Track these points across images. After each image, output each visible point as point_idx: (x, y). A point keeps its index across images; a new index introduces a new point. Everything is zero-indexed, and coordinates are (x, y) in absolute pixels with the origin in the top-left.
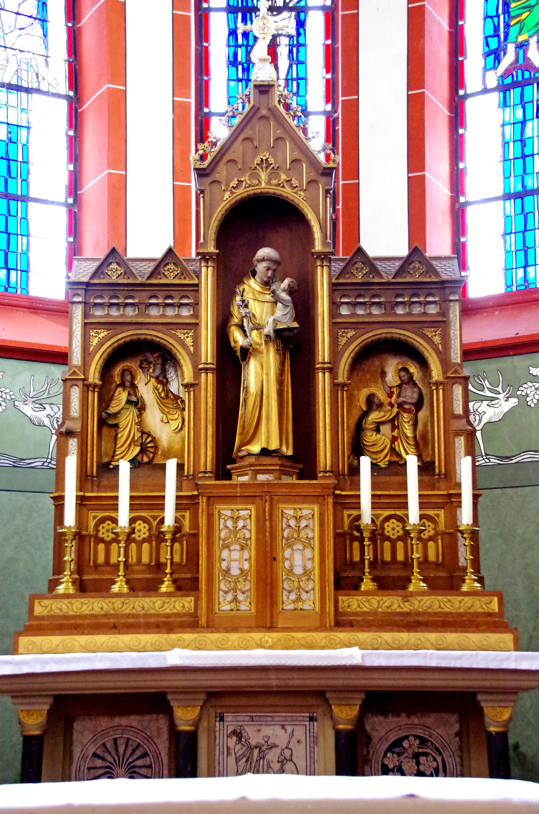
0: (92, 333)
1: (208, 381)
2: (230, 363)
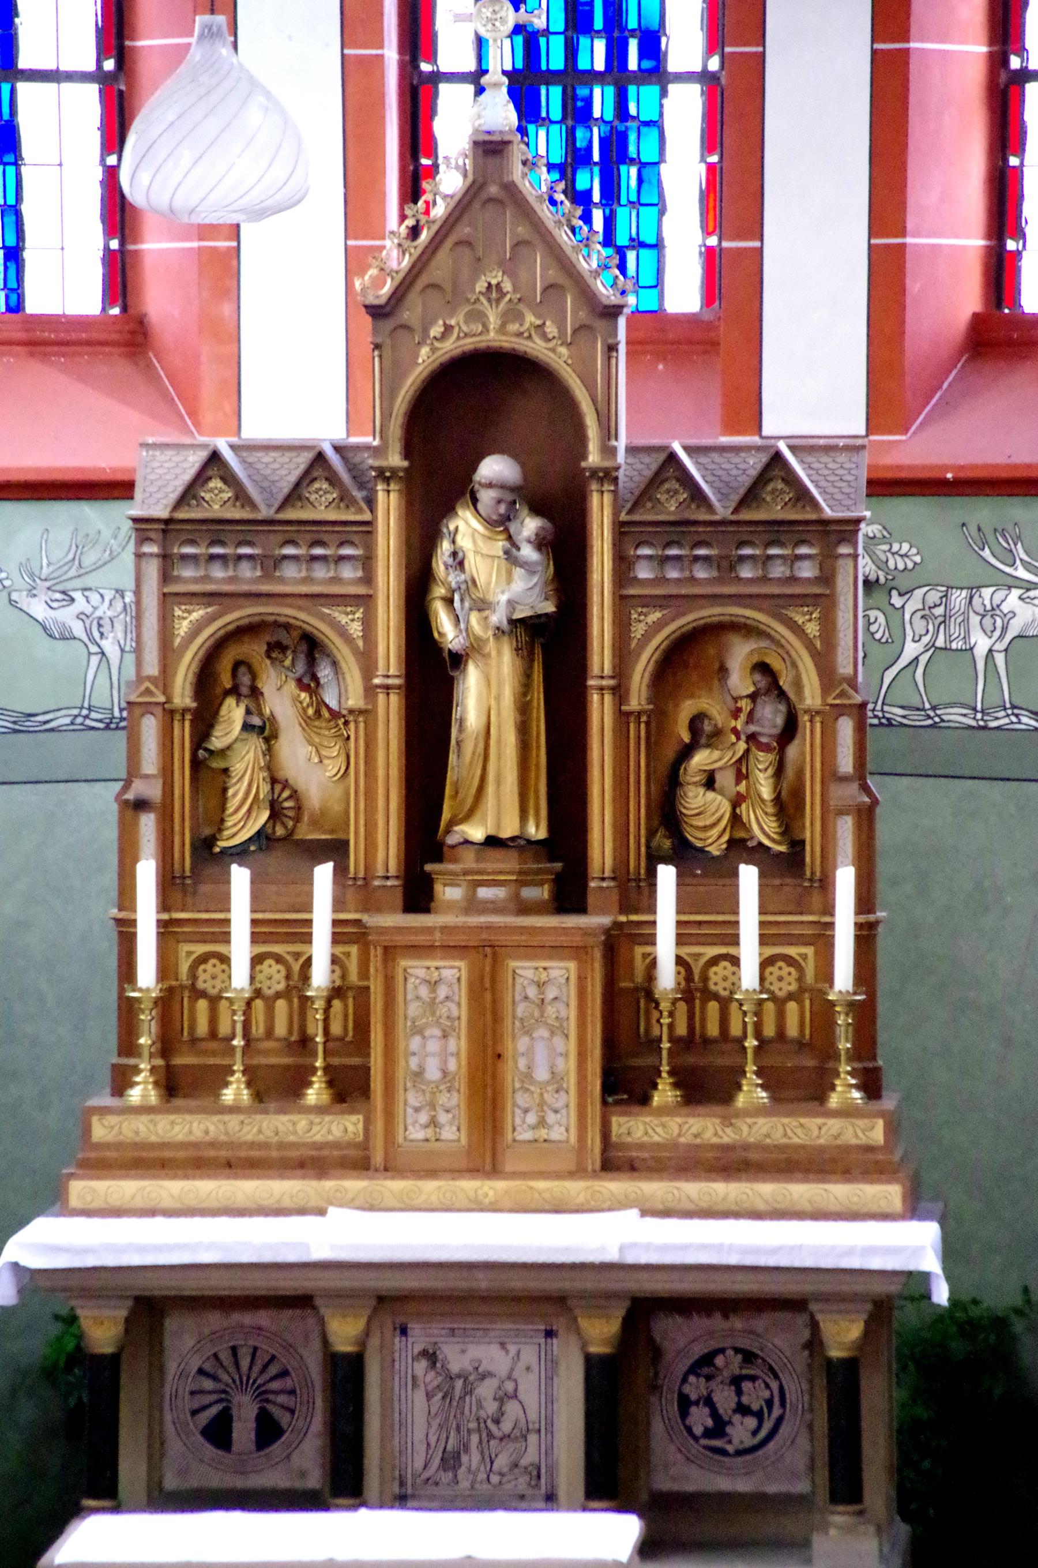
0: (178, 612)
1: (391, 712)
2: (430, 675)
